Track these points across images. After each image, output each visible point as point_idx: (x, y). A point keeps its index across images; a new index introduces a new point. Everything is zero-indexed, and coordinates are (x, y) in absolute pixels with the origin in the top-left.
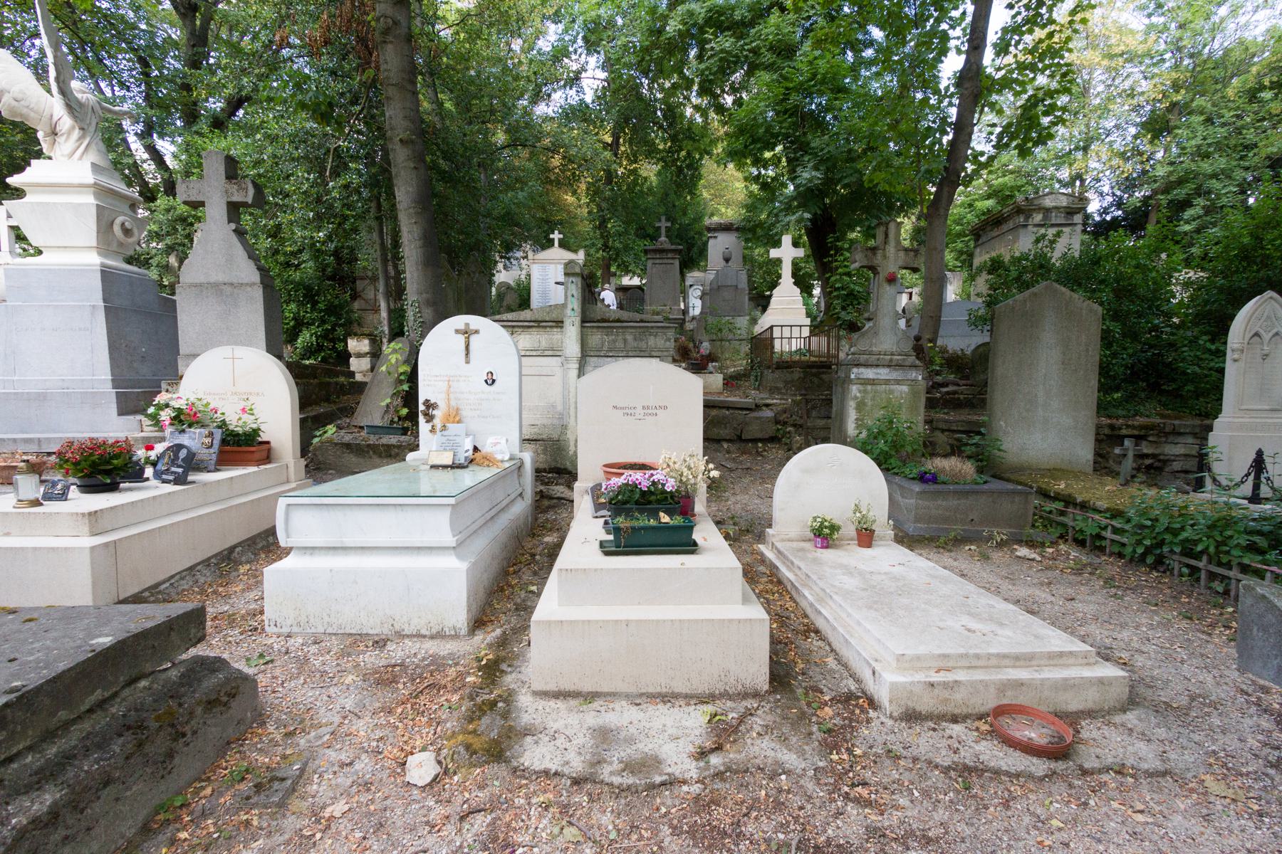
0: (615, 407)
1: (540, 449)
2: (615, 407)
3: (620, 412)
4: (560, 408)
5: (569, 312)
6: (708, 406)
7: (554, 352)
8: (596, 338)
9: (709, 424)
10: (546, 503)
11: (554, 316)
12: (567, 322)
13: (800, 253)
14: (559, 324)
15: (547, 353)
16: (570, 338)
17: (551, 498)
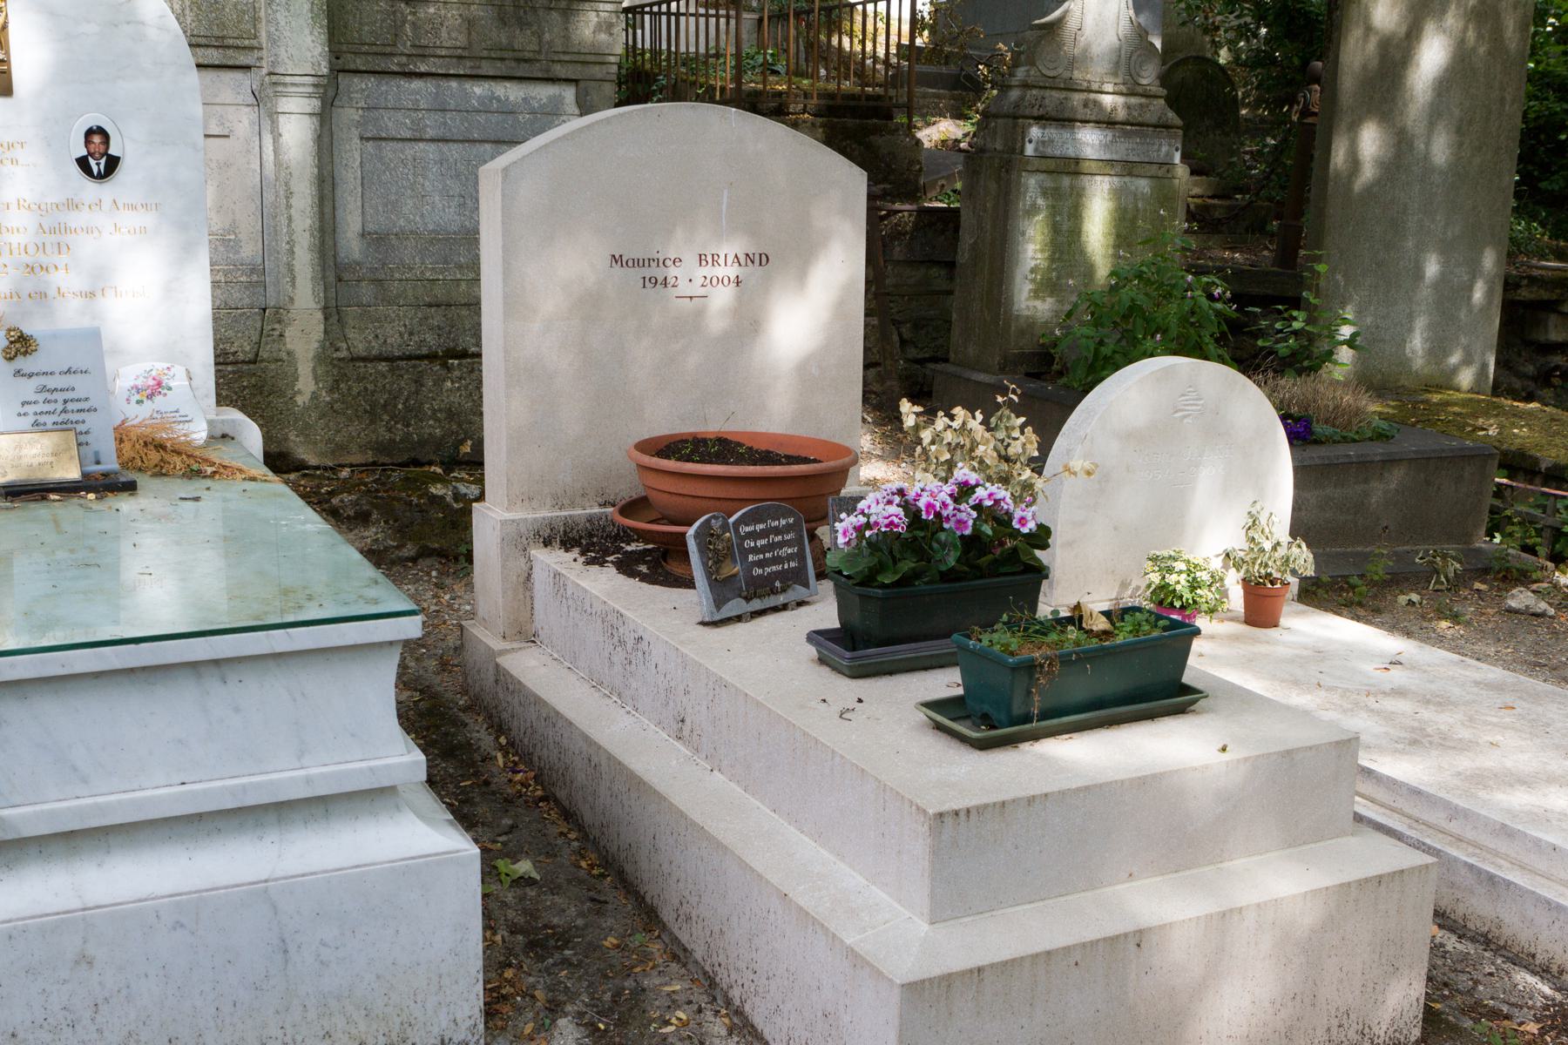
3: (636, 274)
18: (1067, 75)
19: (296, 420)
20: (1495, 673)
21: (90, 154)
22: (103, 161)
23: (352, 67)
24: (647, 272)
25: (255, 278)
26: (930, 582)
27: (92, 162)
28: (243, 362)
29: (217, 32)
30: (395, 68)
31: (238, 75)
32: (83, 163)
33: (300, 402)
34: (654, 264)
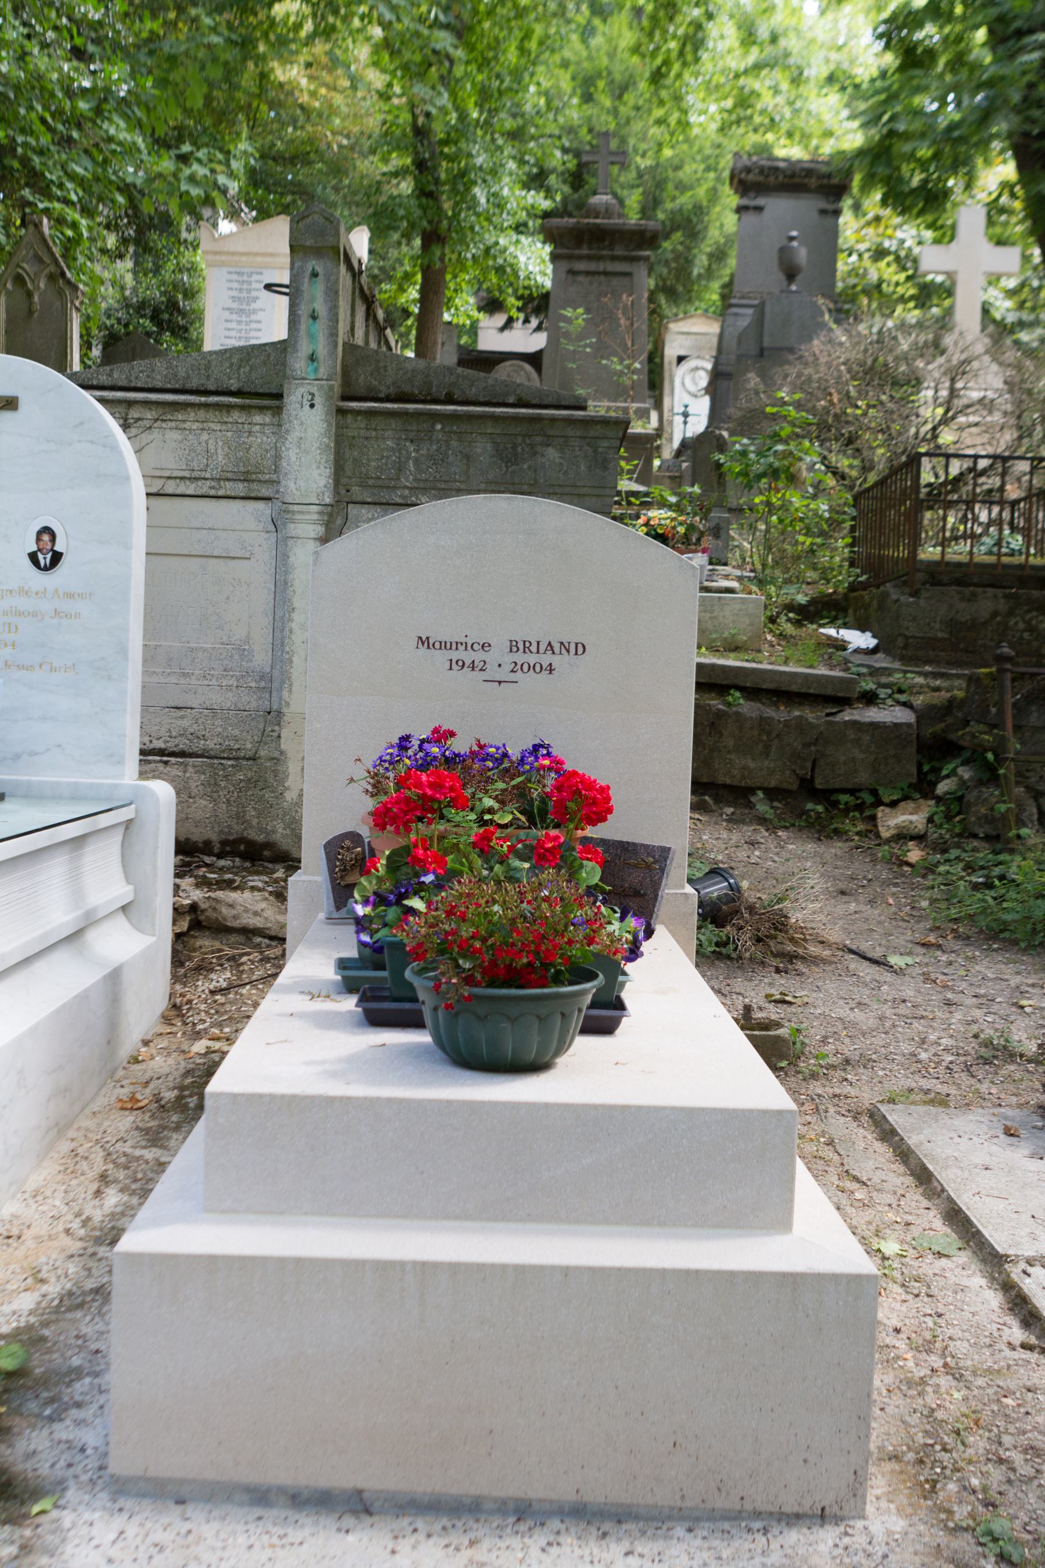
0: (424, 642)
1: (196, 782)
2: (424, 642)
3: (441, 658)
4: (261, 659)
5: (298, 364)
6: (710, 683)
7: (253, 482)
8: (383, 446)
9: (708, 728)
10: (206, 943)
11: (258, 378)
12: (295, 397)
13: (1009, 259)
14: (268, 399)
15: (229, 488)
16: (305, 444)
17: (221, 929)
18: (413, 202)
19: (284, 815)
20: (949, 1231)
21: (39, 550)
22: (49, 556)
23: (360, 499)
24: (455, 655)
25: (263, 684)
26: (583, 993)
27: (40, 556)
28: (244, 758)
29: (242, 469)
30: (398, 500)
31: (260, 505)
32: (33, 557)
33: (288, 799)
34: (461, 648)
